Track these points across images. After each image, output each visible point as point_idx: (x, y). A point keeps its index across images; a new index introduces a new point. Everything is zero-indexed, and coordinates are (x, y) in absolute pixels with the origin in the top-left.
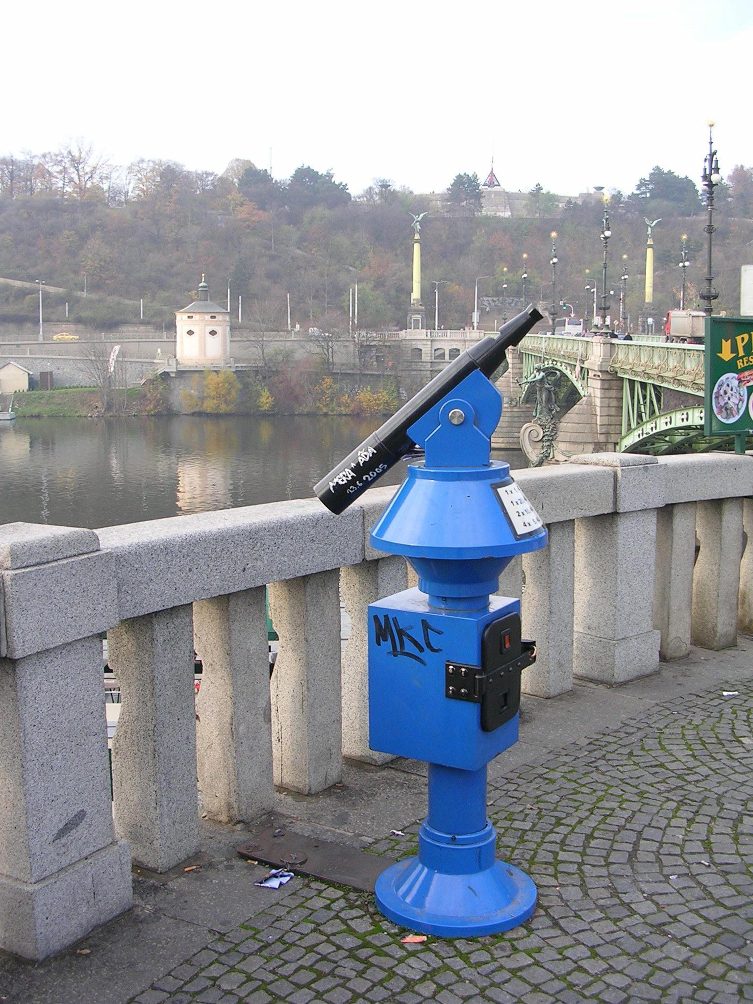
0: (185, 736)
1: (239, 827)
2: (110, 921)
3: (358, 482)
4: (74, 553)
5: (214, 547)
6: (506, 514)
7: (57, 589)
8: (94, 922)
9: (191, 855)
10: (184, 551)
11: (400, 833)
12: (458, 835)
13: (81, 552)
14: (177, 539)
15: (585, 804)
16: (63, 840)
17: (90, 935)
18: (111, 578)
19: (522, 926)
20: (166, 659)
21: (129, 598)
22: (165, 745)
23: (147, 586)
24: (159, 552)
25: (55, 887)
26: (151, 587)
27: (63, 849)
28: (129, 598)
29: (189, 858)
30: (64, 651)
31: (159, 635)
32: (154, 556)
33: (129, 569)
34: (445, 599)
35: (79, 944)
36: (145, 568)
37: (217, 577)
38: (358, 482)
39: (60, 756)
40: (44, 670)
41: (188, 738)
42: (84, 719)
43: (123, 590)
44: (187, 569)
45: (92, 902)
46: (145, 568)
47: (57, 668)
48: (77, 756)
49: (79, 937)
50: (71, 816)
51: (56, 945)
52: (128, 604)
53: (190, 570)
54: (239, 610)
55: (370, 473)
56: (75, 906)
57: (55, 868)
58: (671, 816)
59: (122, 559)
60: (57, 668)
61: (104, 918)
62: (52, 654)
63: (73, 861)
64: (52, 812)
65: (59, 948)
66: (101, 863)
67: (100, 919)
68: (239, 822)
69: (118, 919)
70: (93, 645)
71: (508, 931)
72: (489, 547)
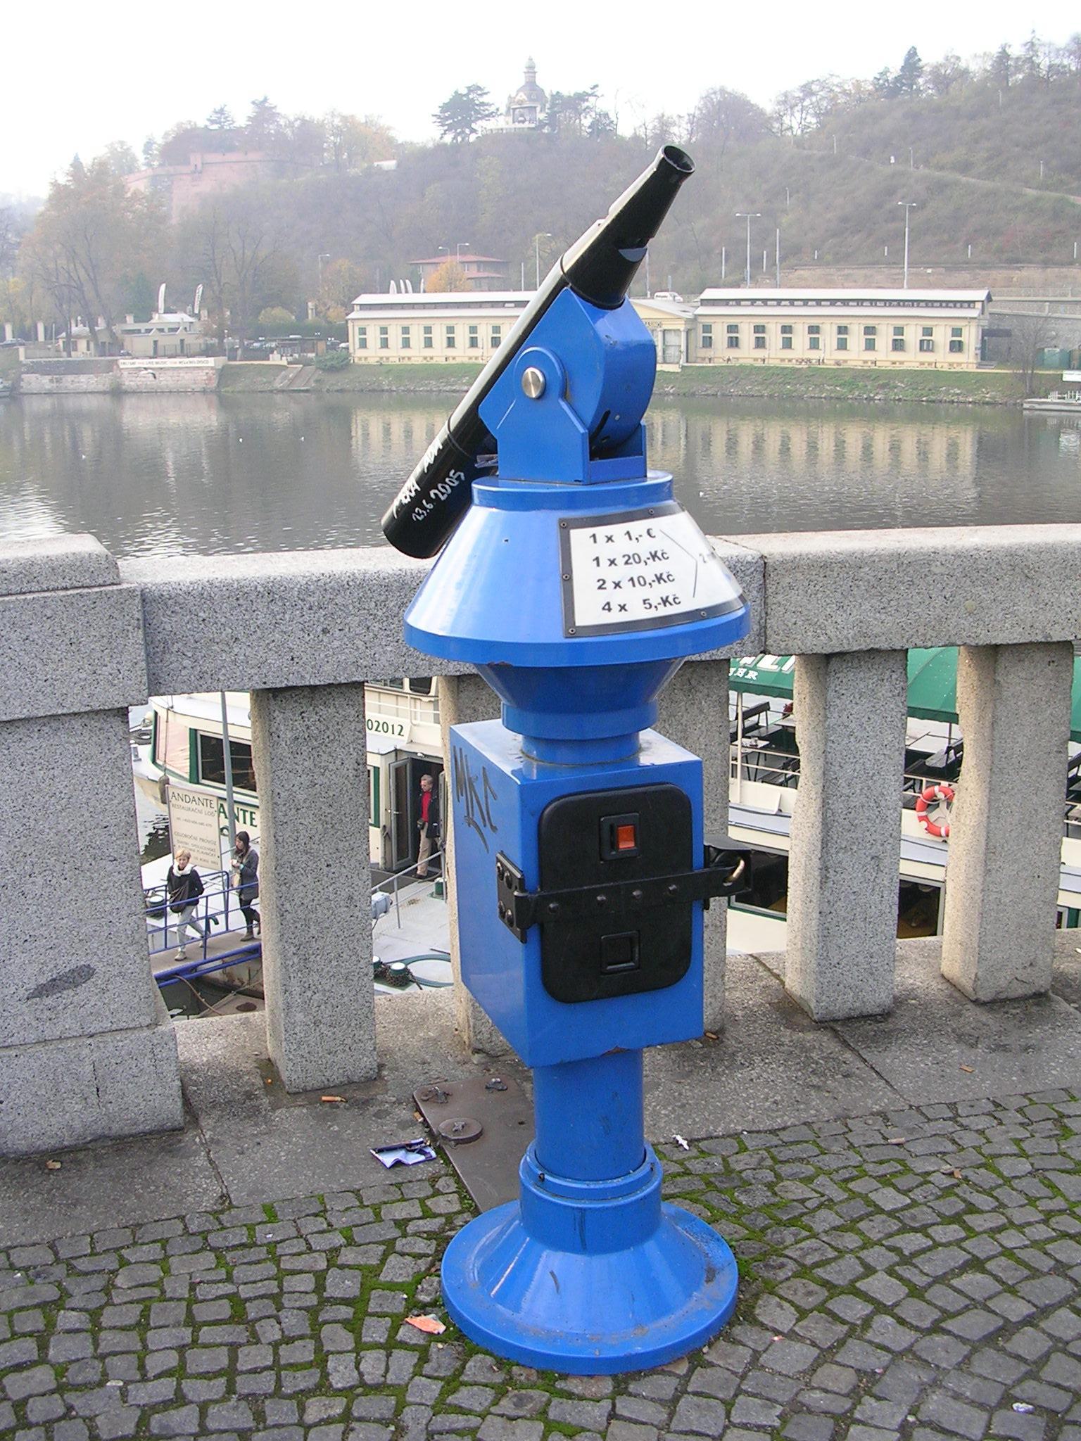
0: (344, 894)
1: (476, 1058)
2: (131, 1135)
3: (424, 502)
4: (64, 585)
5: (383, 598)
6: (567, 580)
7: (13, 636)
8: (98, 1129)
9: (356, 1079)
10: (311, 599)
11: (685, 1143)
12: (552, 1174)
13: (77, 584)
14: (300, 579)
15: (1059, 1198)
16: (49, 1001)
17: (89, 1146)
18: (130, 628)
19: (614, 1377)
20: (300, 769)
21: (186, 662)
22: (298, 901)
23: (227, 649)
24: (253, 597)
25: (16, 1062)
26: (236, 650)
27: (48, 1013)
28: (186, 662)
29: (351, 1083)
30: (46, 729)
31: (282, 727)
32: (241, 602)
33: (186, 619)
34: (536, 738)
35: (58, 1153)
36: (223, 620)
37: (389, 649)
38: (424, 502)
39: (40, 880)
40: (6, 752)
41: (350, 898)
42: (90, 833)
43: (175, 648)
44: (319, 629)
45: (93, 1099)
46: (223, 620)
47: (33, 751)
48: (76, 885)
49: (66, 1143)
50: (63, 970)
51: (23, 1146)
52: (183, 673)
53: (325, 631)
54: (481, 708)
55: (439, 486)
56: (58, 1097)
57: (32, 1037)
58: (322, 1265)
59: (170, 602)
60: (33, 751)
61: (116, 1129)
62: (22, 730)
63: (67, 1035)
64: (24, 958)
65: (25, 1149)
66: (111, 1049)
67: (110, 1128)
68: (477, 1051)
69: (148, 1137)
70: (107, 726)
71: (576, 1376)
72: (529, 644)
